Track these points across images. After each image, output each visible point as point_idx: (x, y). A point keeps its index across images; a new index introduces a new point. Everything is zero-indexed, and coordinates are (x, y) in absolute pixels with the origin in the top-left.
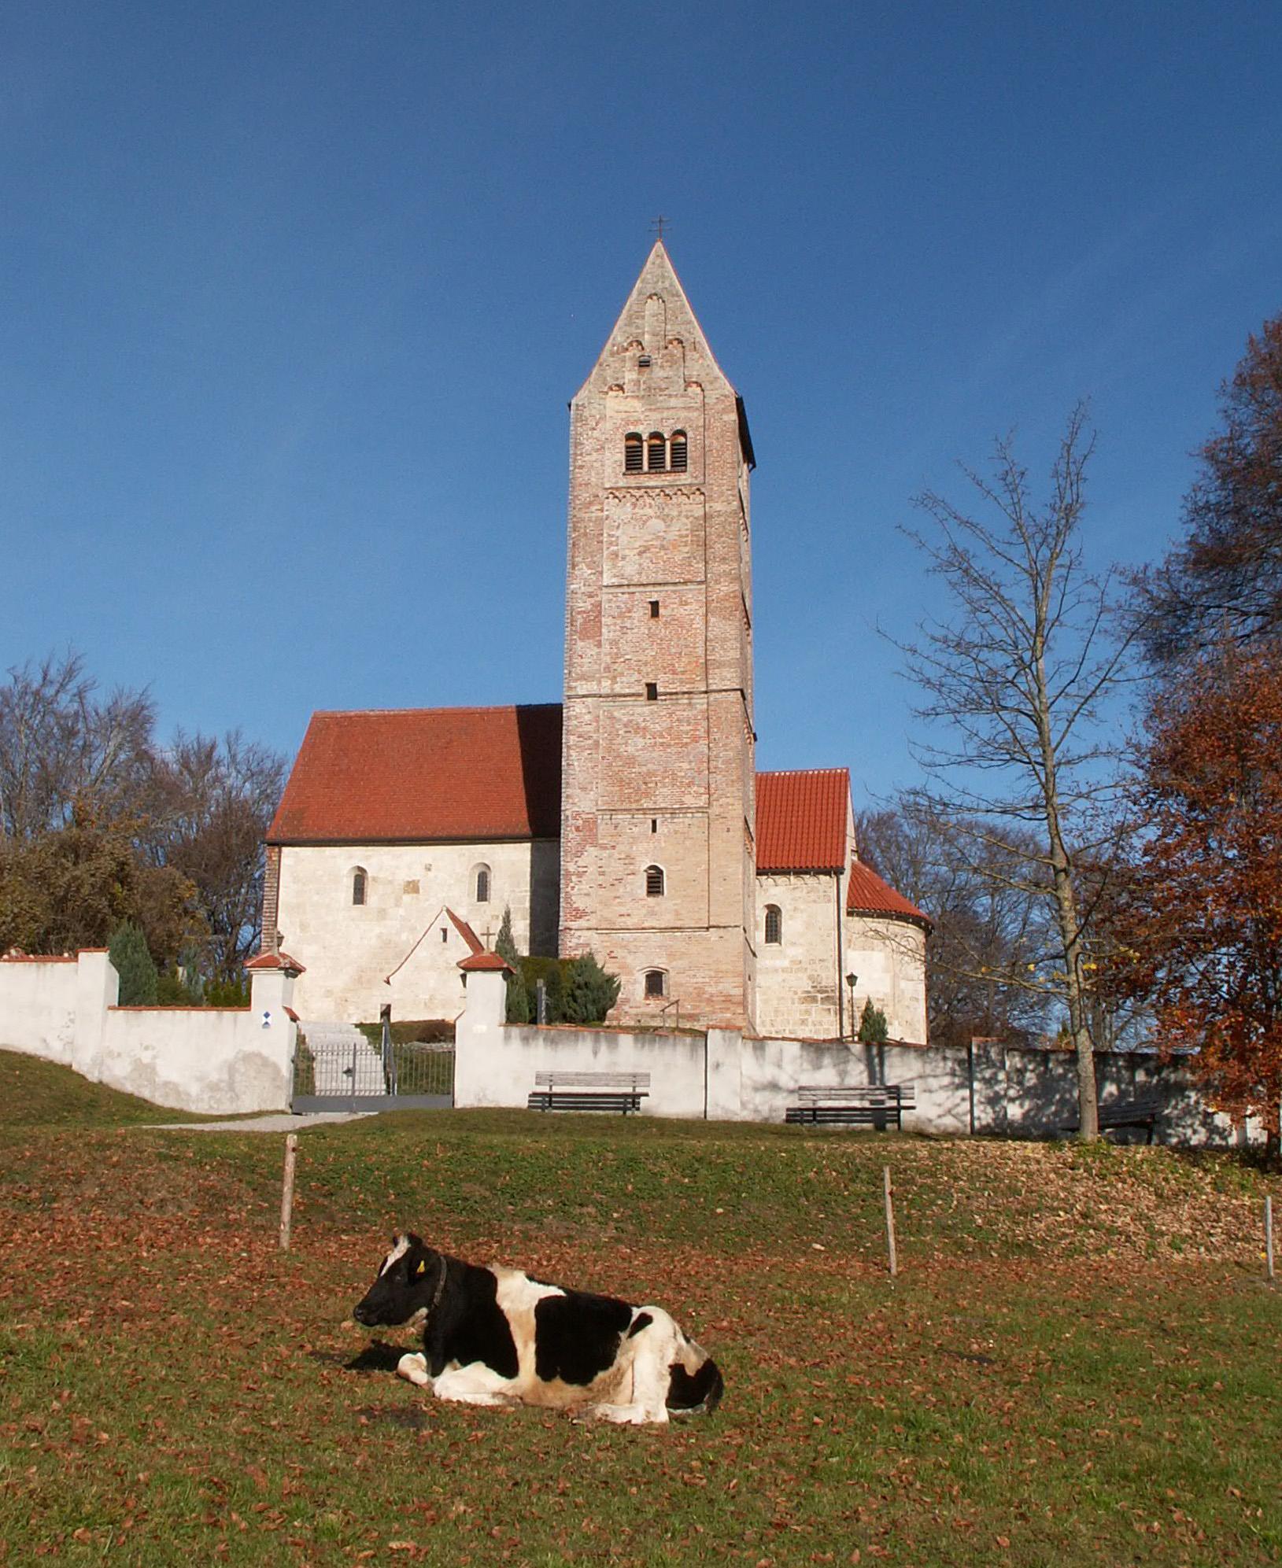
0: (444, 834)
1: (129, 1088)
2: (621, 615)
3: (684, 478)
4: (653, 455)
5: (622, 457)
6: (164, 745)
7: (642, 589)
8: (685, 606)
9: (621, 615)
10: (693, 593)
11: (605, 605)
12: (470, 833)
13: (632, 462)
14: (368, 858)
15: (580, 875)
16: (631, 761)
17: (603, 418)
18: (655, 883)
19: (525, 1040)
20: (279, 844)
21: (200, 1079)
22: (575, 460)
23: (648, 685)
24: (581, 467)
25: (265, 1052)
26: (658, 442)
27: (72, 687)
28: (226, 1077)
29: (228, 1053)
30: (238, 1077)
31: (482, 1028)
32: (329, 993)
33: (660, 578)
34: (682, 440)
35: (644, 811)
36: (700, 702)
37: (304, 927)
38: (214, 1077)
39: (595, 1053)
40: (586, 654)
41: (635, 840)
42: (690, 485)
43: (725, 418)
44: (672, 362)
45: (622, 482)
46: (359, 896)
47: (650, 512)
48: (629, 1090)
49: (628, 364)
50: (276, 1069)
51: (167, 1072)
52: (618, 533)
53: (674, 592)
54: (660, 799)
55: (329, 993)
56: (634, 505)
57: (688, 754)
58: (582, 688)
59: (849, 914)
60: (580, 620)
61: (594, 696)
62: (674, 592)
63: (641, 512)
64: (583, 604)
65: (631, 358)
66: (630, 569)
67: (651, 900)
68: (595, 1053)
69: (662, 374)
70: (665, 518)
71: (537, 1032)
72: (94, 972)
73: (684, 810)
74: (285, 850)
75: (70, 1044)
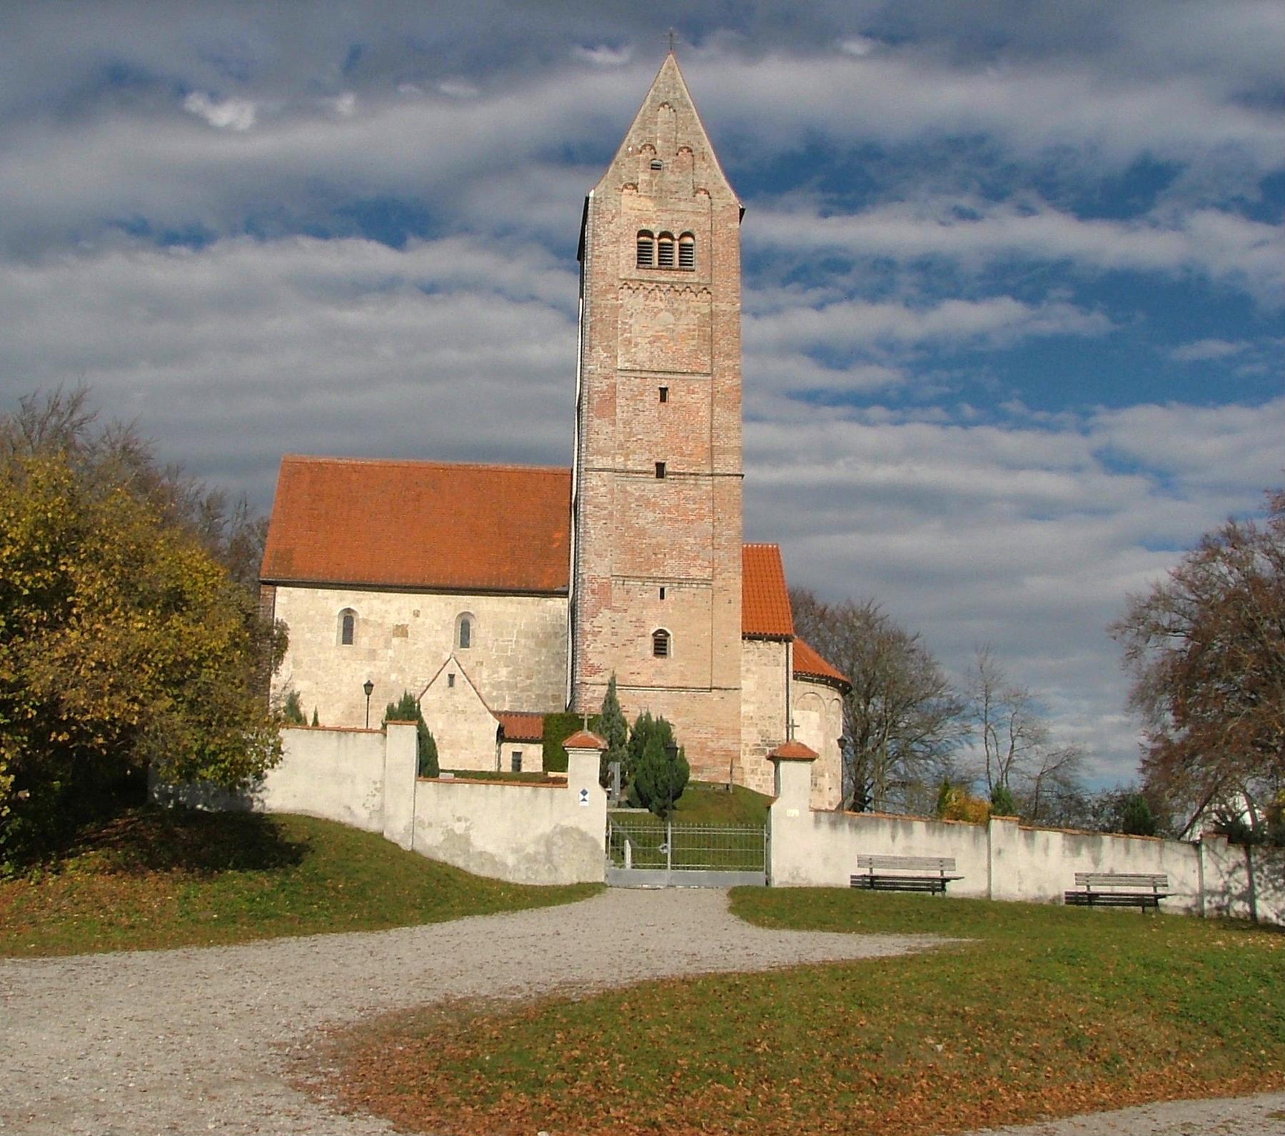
0: (433, 582)
1: (441, 856)
2: (633, 398)
3: (691, 277)
4: (660, 251)
7: (652, 375)
8: (692, 396)
9: (633, 398)
10: (700, 384)
12: (456, 584)
14: (359, 601)
15: (595, 634)
16: (642, 532)
17: (618, 213)
18: (660, 645)
21: (516, 851)
22: (593, 250)
23: (657, 464)
24: (598, 257)
25: (583, 827)
26: (669, 241)
28: (543, 849)
29: (545, 827)
30: (555, 850)
31: (793, 812)
33: (670, 367)
34: (689, 240)
36: (706, 484)
38: (531, 849)
39: (893, 838)
40: (601, 430)
41: (645, 605)
42: (699, 284)
43: (731, 225)
45: (636, 274)
46: (348, 635)
47: (661, 305)
48: (937, 874)
49: (642, 166)
51: (481, 842)
52: (631, 322)
53: (683, 381)
54: (668, 569)
56: (646, 297)
57: (694, 530)
58: (599, 462)
59: (795, 678)
61: (610, 470)
62: (683, 381)
63: (653, 304)
64: (600, 385)
65: (644, 161)
66: (642, 356)
67: (659, 660)
68: (893, 838)
69: (672, 178)
70: (674, 312)
71: (843, 816)
73: (690, 581)
74: (279, 589)
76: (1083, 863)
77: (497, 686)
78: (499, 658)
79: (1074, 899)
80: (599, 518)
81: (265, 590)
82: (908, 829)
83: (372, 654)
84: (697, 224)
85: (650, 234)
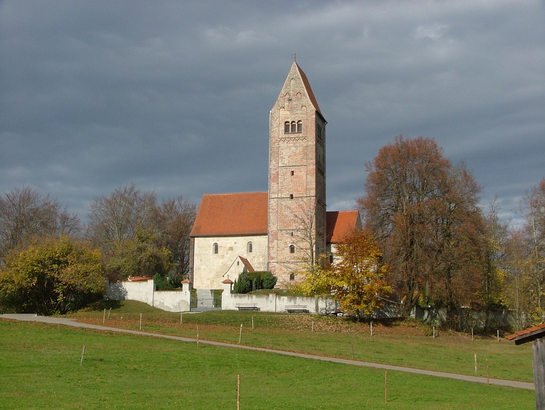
1: (159, 307)
2: (284, 175)
3: (301, 135)
5: (284, 128)
6: (159, 203)
9: (284, 175)
10: (303, 169)
11: (279, 172)
12: (247, 233)
13: (286, 130)
14: (219, 240)
15: (272, 248)
19: (235, 297)
20: (194, 237)
27: (133, 193)
29: (178, 300)
31: (227, 295)
32: (209, 279)
33: (294, 164)
34: (294, 123)
35: (290, 230)
37: (201, 260)
38: (176, 305)
46: (216, 251)
47: (291, 145)
51: (166, 304)
55: (209, 279)
58: (273, 196)
60: (272, 176)
64: (273, 172)
66: (286, 162)
70: (296, 147)
72: (151, 283)
75: (147, 298)
76: (292, 303)
77: (259, 263)
78: (260, 255)
80: (274, 213)
81: (192, 239)
82: (252, 297)
83: (223, 256)
85: (288, 122)
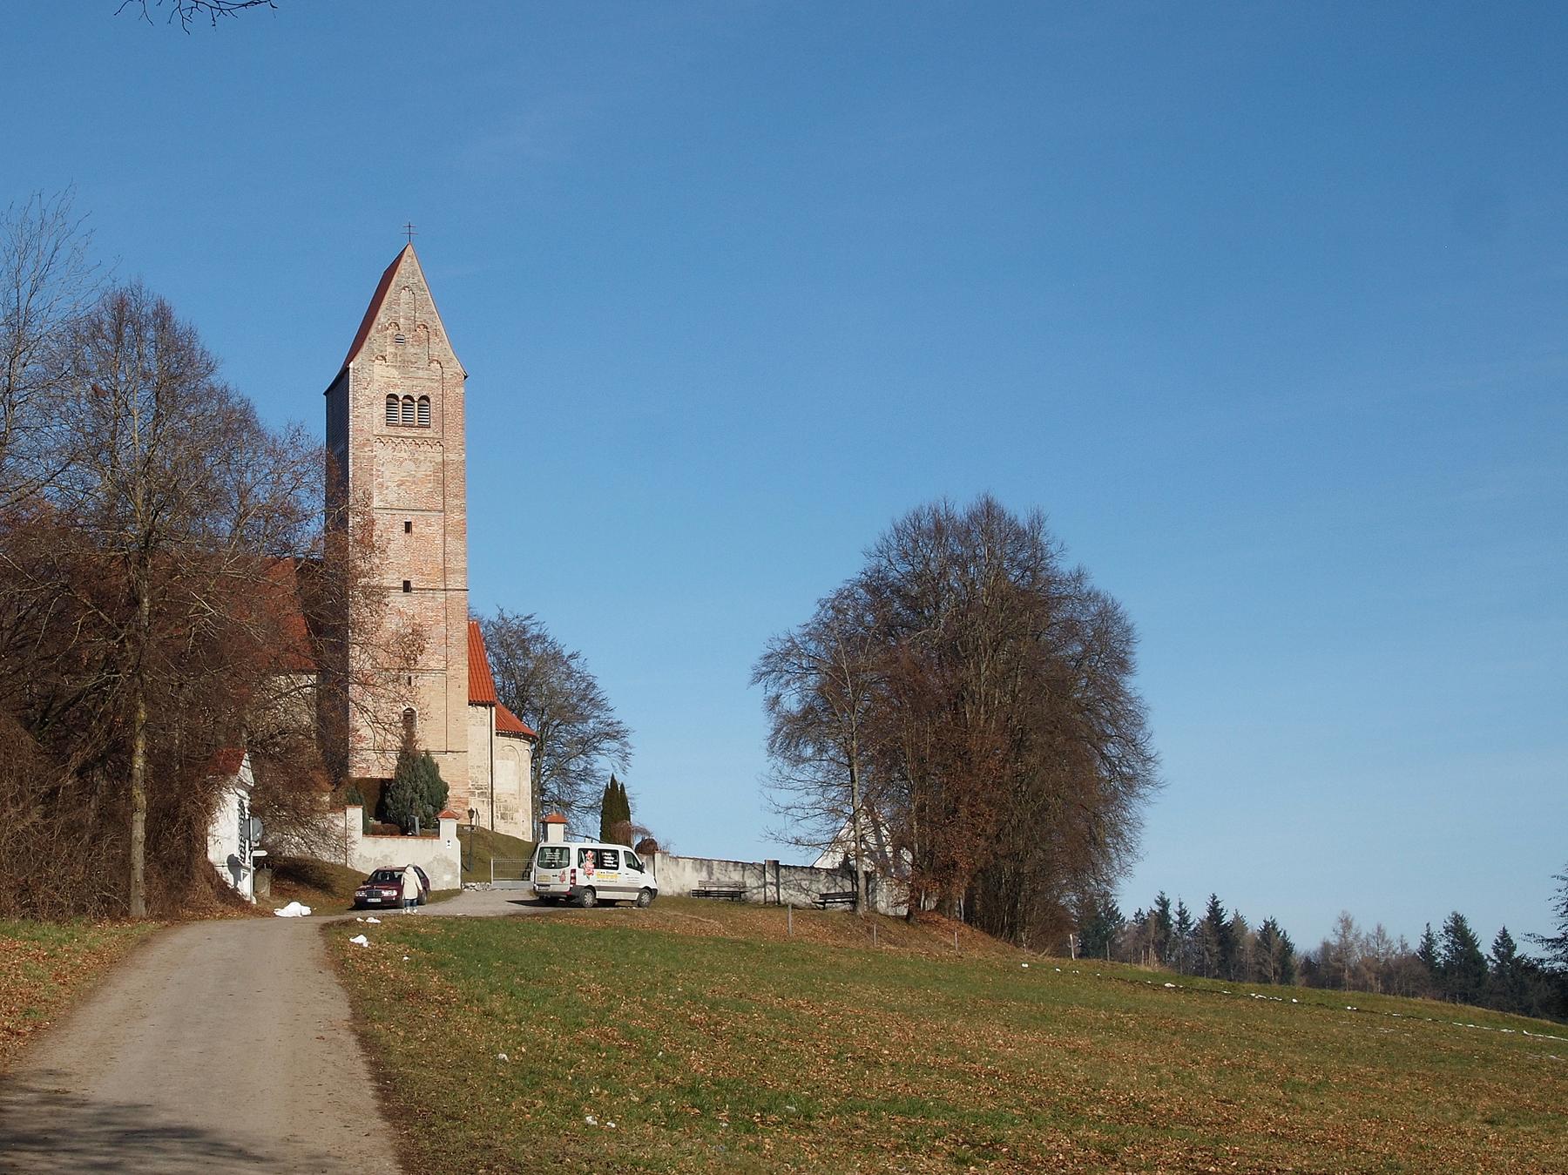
3: (428, 433)
8: (429, 527)
33: (412, 505)
36: (440, 596)
44: (419, 341)
45: (386, 431)
47: (403, 454)
50: (453, 865)
66: (392, 497)
70: (415, 461)
79: (698, 893)
84: (432, 389)
85: (396, 397)
